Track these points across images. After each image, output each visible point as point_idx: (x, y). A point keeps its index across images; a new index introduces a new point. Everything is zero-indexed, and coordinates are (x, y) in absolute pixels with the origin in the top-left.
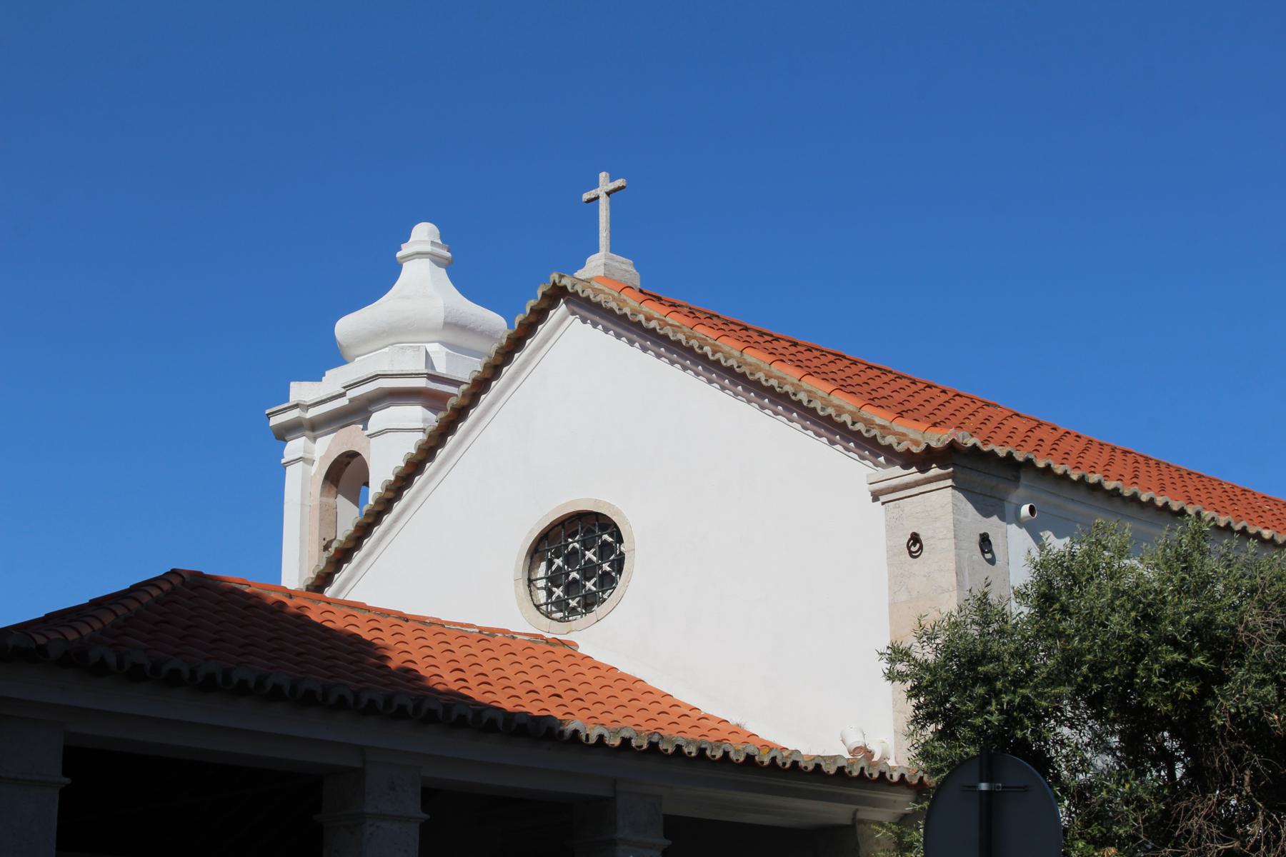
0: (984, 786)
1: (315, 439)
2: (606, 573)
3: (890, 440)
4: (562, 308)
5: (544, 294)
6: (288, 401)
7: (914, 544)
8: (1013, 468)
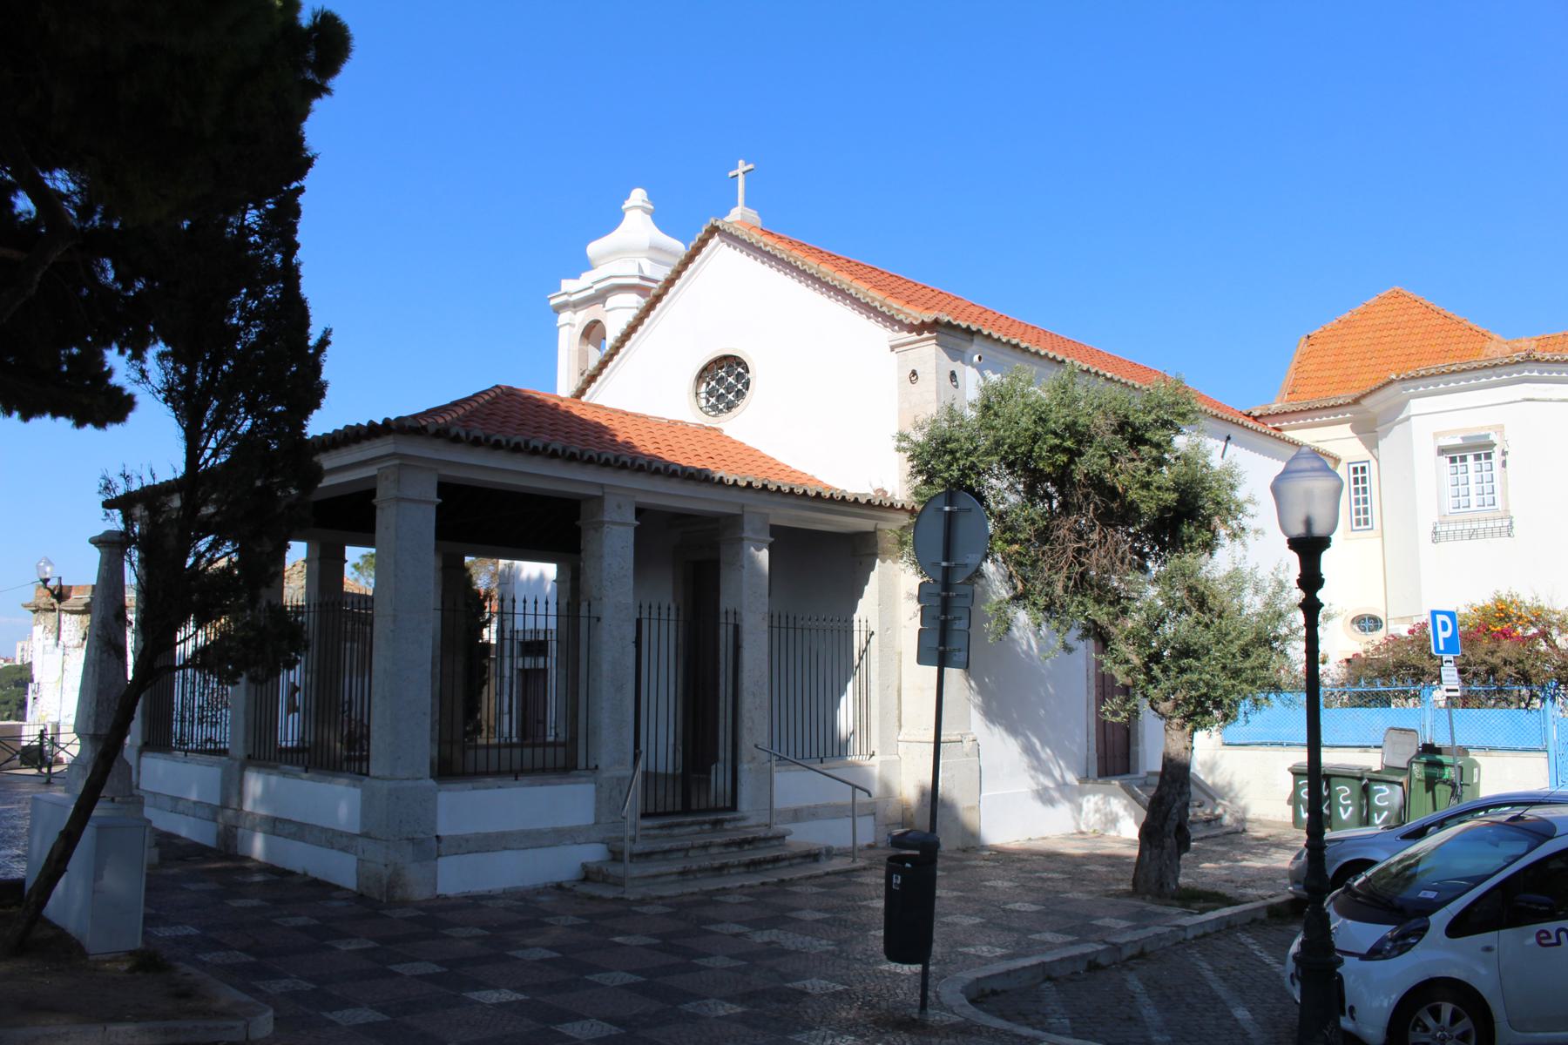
0: (947, 509)
1: (575, 313)
2: (739, 390)
3: (901, 317)
4: (717, 238)
6: (560, 290)
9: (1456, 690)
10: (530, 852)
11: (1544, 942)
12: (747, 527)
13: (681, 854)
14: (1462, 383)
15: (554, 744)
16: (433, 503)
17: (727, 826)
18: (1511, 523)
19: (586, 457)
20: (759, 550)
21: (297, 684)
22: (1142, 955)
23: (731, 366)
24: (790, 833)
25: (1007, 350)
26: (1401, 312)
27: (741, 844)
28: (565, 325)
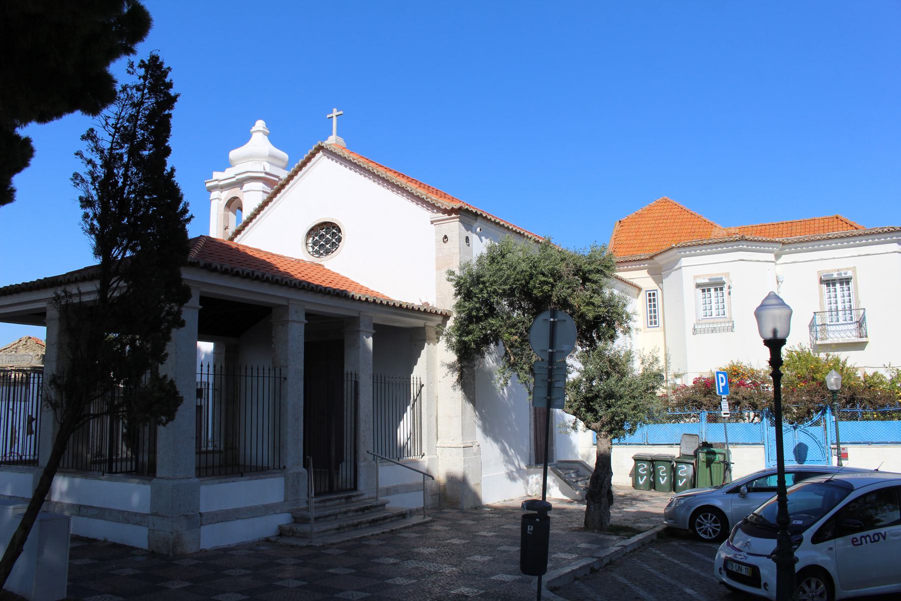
0: (552, 320)
1: (222, 192)
2: (333, 242)
3: (439, 205)
4: (321, 153)
5: (315, 148)
6: (212, 178)
7: (445, 239)
8: (476, 215)
9: (728, 414)
10: (251, 520)
11: (855, 543)
12: (361, 324)
13: (334, 517)
14: (709, 250)
15: (213, 452)
16: (196, 308)
17: (353, 499)
18: (733, 324)
19: (284, 283)
20: (368, 337)
21: (34, 416)
22: (611, 563)
23: (328, 228)
24: (388, 502)
25: (493, 225)
26: (668, 210)
27: (363, 510)
28: (215, 199)
